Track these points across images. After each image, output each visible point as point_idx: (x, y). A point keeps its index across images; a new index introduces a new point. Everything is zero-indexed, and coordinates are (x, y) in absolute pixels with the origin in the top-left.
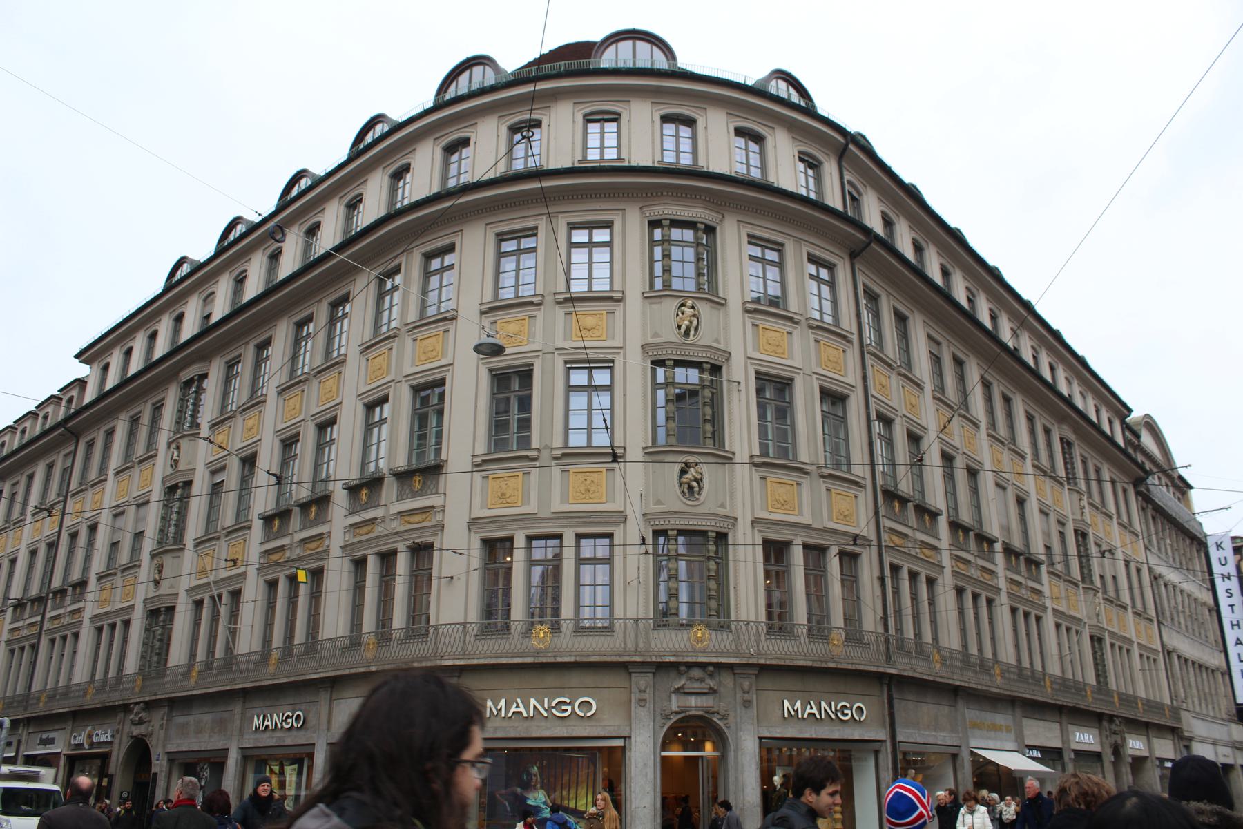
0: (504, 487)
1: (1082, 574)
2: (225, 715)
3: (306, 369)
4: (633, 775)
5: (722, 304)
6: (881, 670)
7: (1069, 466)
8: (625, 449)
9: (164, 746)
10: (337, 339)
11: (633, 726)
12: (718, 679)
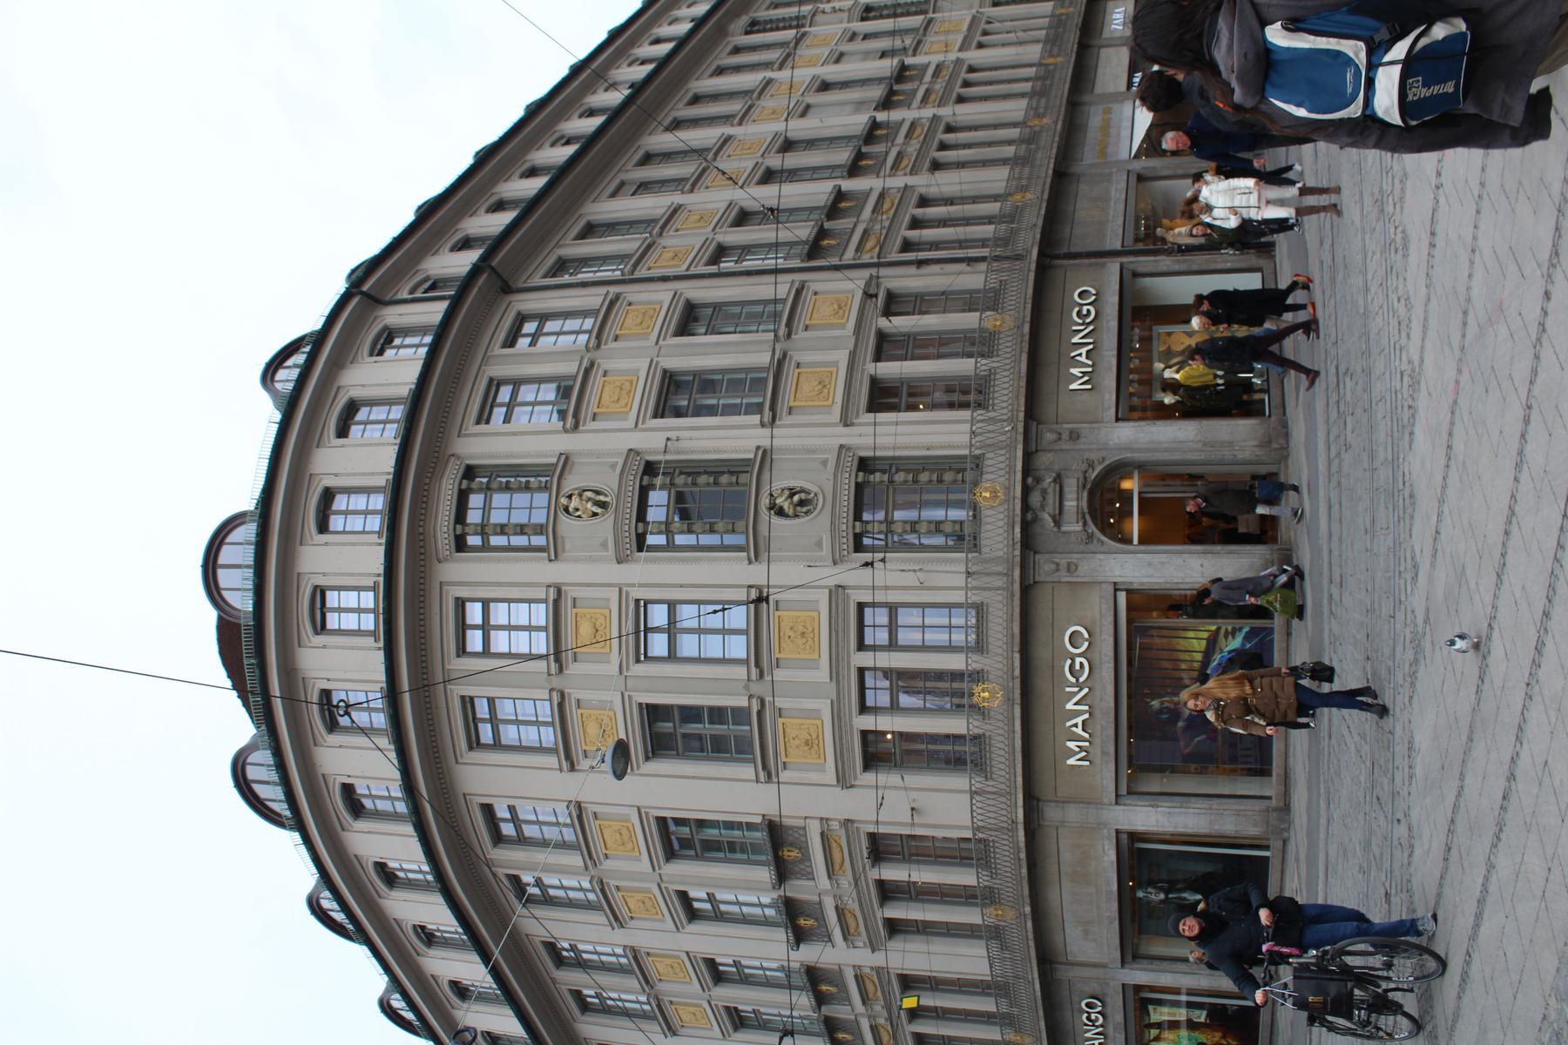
0: (797, 742)
1: (916, 13)
3: (643, 998)
6: (1033, 266)
7: (781, 25)
8: (750, 587)
10: (604, 958)
11: (1101, 579)
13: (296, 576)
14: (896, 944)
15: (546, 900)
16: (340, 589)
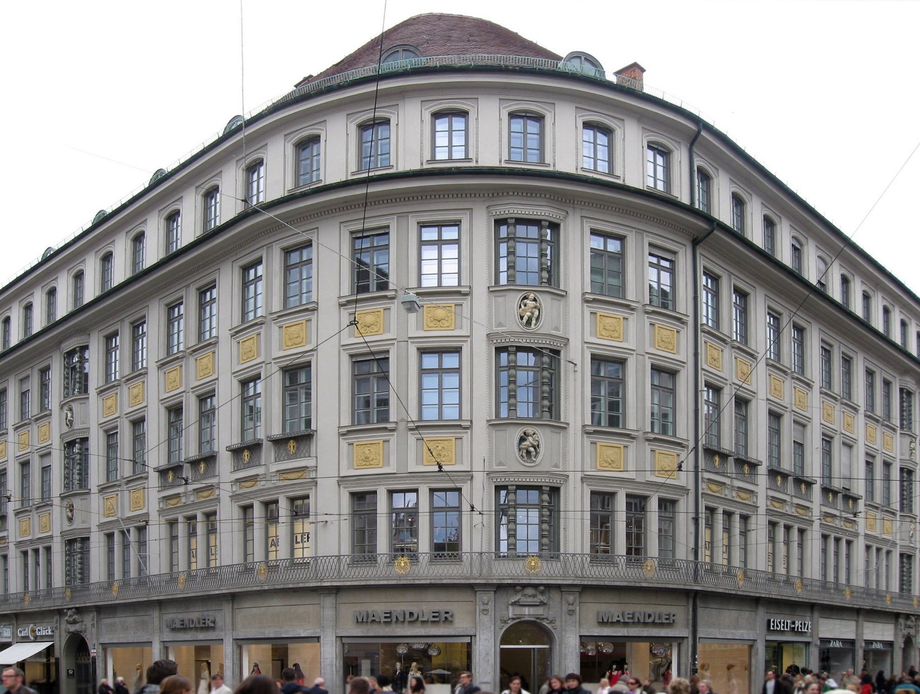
0: (367, 452)
2: (146, 618)
3: (182, 348)
4: (477, 661)
5: (562, 296)
6: (688, 587)
8: (471, 422)
9: (98, 639)
10: (208, 321)
11: (478, 628)
12: (548, 595)
13: (475, 96)
14: (237, 513)
15: (245, 284)
16: (466, 130)
